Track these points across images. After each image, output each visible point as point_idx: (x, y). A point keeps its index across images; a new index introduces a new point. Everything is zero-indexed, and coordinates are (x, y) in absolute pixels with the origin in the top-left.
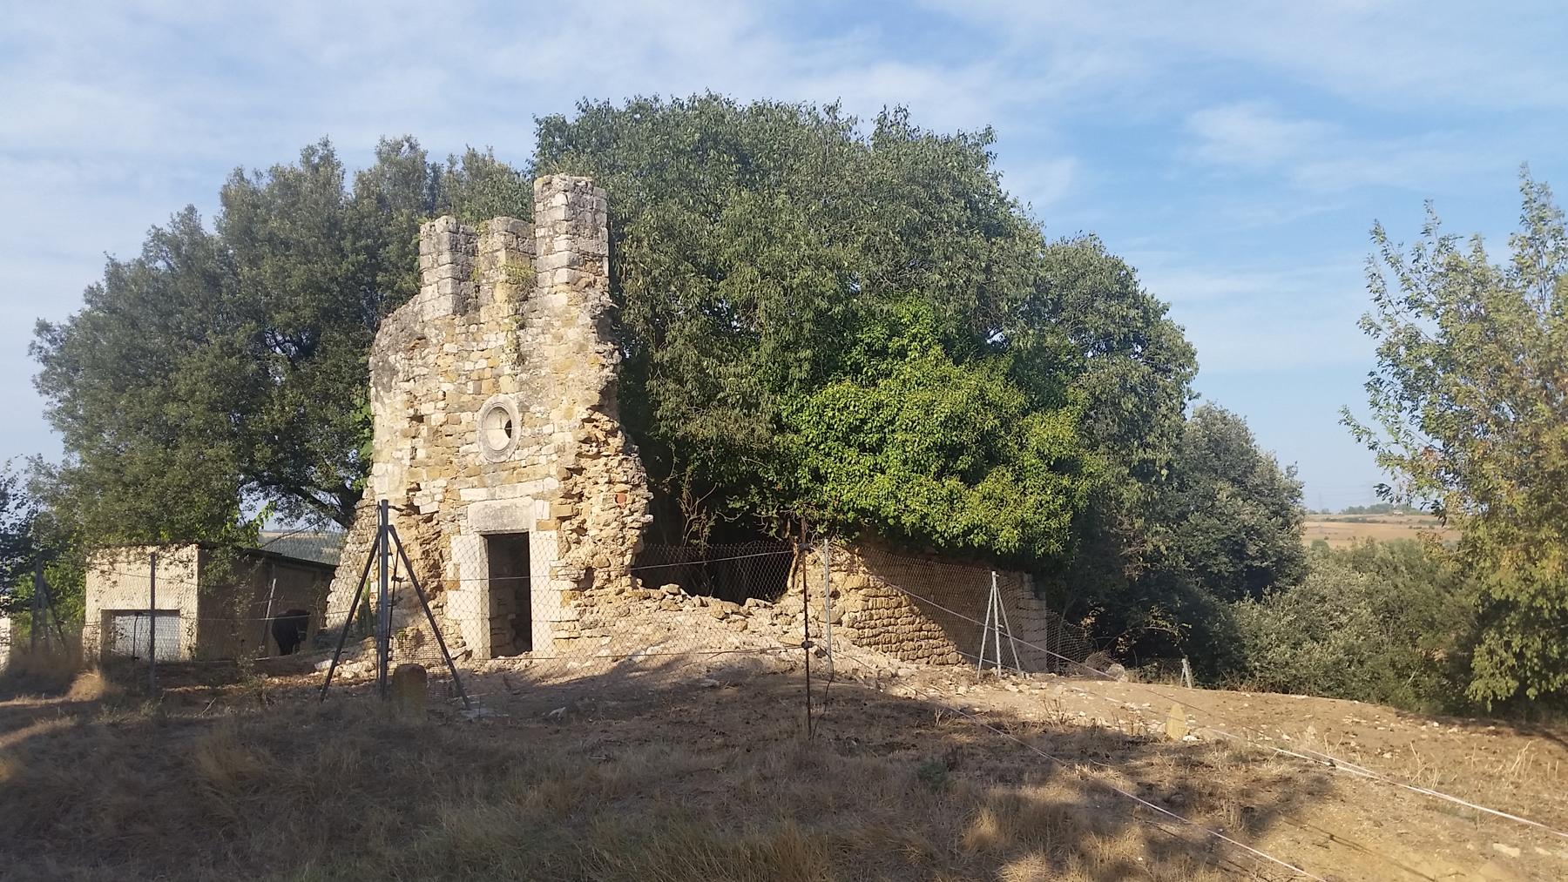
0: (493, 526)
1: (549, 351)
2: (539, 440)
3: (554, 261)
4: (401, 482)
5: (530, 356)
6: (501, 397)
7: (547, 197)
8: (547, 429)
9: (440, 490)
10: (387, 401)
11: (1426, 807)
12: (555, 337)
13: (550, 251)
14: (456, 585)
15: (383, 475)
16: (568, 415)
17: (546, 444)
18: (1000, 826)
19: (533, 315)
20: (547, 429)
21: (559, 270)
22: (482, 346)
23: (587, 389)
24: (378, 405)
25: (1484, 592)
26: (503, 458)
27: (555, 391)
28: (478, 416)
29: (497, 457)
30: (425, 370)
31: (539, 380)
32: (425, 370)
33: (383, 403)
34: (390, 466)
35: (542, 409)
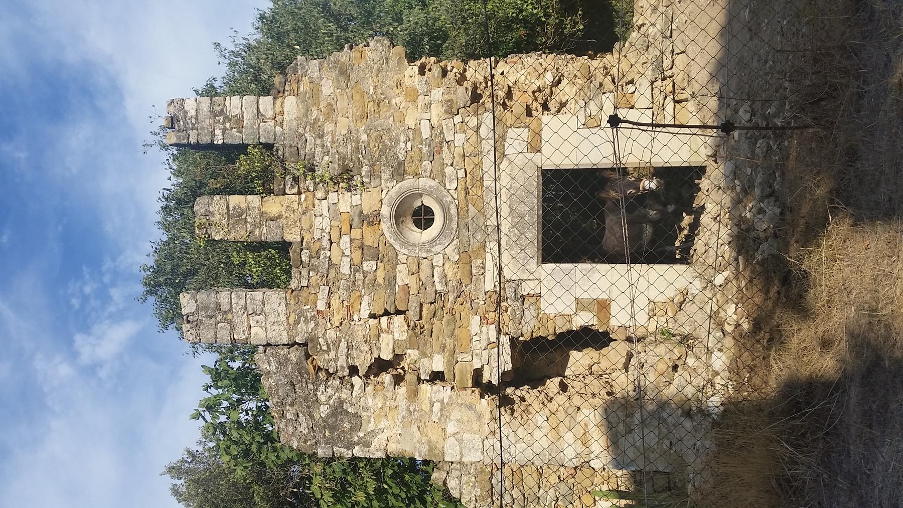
0: (533, 250)
1: (343, 125)
2: (438, 143)
3: (251, 115)
4: (470, 407)
5: (344, 159)
6: (385, 211)
7: (185, 123)
8: (426, 133)
9: (484, 329)
10: (371, 427)
11: (627, 371)
12: (328, 117)
13: (239, 122)
14: (603, 307)
15: (460, 441)
16: (412, 96)
17: (442, 132)
18: (801, 296)
19: (302, 152)
20: (426, 133)
21: (261, 109)
22: (325, 243)
23: (387, 63)
24: (375, 443)
25: (260, 213)
26: (453, 211)
27: (385, 120)
28: (403, 251)
29: (451, 220)
30: (343, 345)
31: (372, 145)
32: (343, 345)
33: (373, 434)
34: (451, 428)
35: (403, 138)
